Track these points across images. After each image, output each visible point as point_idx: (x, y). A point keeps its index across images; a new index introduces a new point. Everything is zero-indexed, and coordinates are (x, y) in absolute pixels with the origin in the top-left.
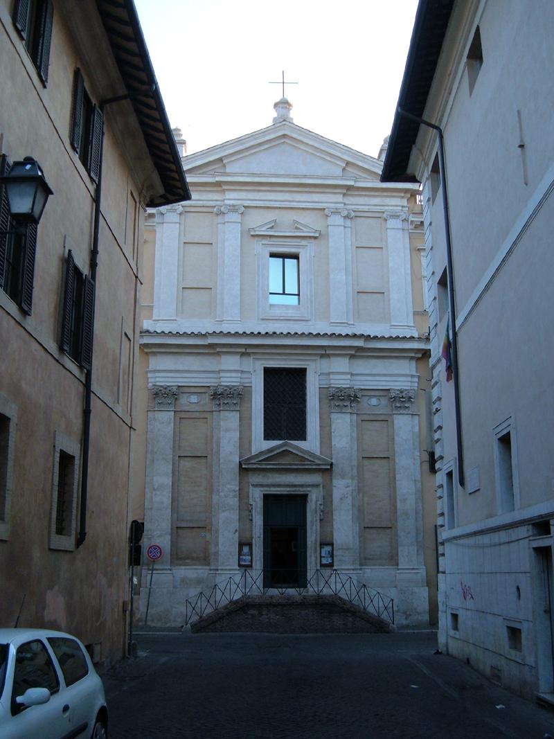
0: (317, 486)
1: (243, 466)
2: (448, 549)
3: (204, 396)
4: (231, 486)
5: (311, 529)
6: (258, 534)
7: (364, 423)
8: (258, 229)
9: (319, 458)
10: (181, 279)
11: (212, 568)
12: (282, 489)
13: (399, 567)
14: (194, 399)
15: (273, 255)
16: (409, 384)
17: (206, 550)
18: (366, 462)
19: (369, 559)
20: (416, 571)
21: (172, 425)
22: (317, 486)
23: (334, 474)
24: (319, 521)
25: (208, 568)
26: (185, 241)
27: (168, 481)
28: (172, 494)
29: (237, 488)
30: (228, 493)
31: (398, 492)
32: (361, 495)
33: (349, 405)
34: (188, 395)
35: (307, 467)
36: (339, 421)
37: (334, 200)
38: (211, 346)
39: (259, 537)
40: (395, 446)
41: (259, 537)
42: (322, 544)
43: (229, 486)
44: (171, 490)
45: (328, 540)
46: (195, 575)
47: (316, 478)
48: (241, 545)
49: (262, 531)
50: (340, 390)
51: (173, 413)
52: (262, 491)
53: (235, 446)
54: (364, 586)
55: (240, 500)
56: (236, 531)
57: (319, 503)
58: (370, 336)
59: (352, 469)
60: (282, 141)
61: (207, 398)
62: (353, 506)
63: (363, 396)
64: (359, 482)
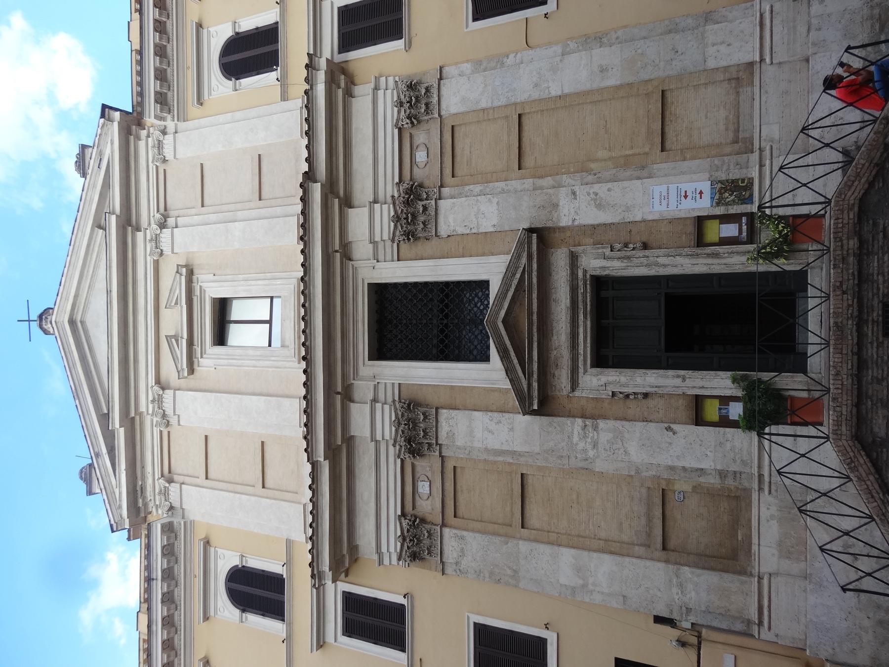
0: (574, 259)
1: (535, 407)
2: (852, 218)
3: (419, 469)
4: (576, 432)
5: (665, 266)
6: (678, 382)
7: (458, 172)
8: (179, 366)
9: (516, 257)
10: (250, 490)
11: (756, 486)
12: (581, 330)
13: (758, 60)
14: (423, 488)
15: (220, 338)
16: (389, 92)
17: (712, 495)
18: (528, 161)
19: (737, 131)
20: (767, 15)
21: (465, 533)
22: (574, 259)
23: (550, 224)
24: (647, 253)
25: (755, 496)
26: (204, 477)
27: (567, 555)
28: (595, 551)
29: (579, 421)
30: (589, 440)
31: (588, 86)
32: (593, 166)
33: (424, 203)
34: (417, 497)
35: (535, 280)
36: (451, 220)
37: (142, 243)
38: (332, 452)
39: (684, 380)
40: (496, 104)
41: (684, 380)
42: (700, 242)
43: (576, 439)
44: (585, 553)
45: (691, 229)
46: (774, 524)
47: (560, 260)
48: (699, 420)
49: (671, 373)
50: (397, 219)
51: (446, 531)
52: (585, 371)
53: (499, 422)
54: (804, 129)
55: (605, 417)
56: (668, 429)
57: (607, 251)
58: (306, 172)
59: (541, 188)
60: (79, 325)
61: (422, 465)
62: (614, 180)
63: (411, 179)
64: (568, 173)
